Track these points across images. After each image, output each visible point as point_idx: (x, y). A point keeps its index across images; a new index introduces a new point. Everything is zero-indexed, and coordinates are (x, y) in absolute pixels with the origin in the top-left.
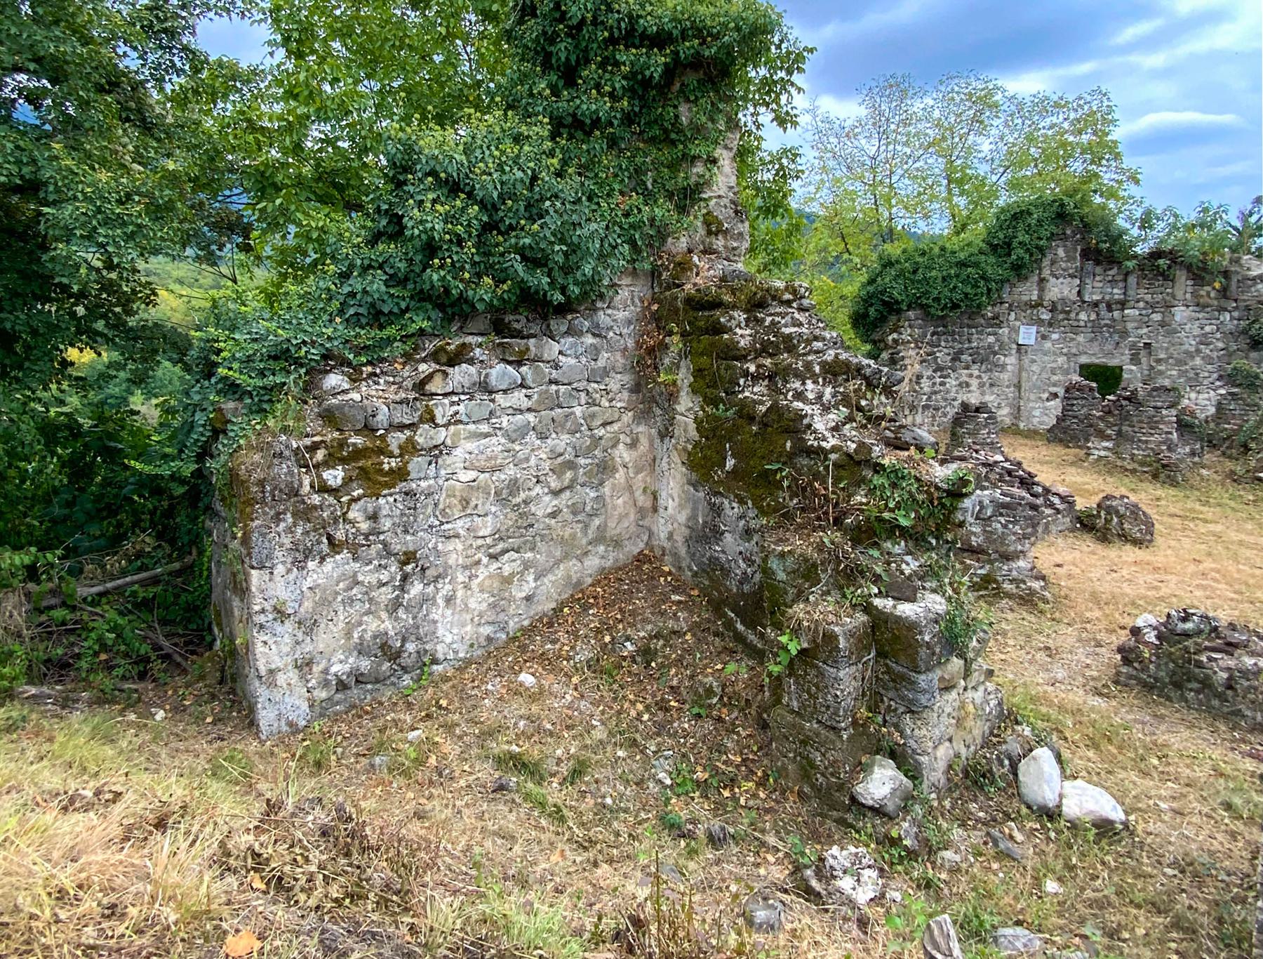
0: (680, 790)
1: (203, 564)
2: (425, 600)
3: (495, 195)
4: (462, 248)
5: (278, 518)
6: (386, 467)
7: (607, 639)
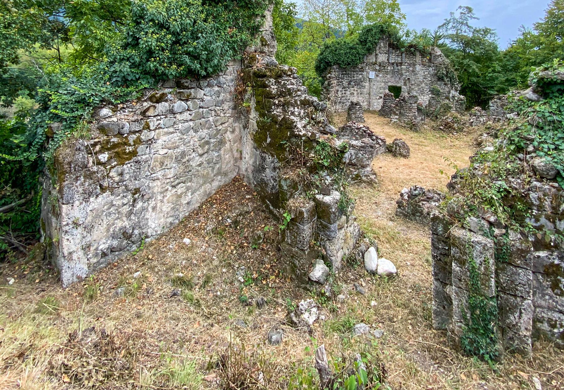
0: (247, 284)
1: (37, 199)
2: (144, 209)
3: (178, 30)
4: (164, 53)
5: (77, 179)
6: (127, 151)
7: (220, 218)
